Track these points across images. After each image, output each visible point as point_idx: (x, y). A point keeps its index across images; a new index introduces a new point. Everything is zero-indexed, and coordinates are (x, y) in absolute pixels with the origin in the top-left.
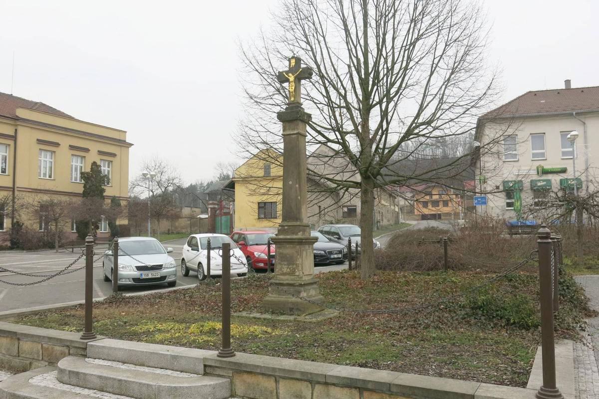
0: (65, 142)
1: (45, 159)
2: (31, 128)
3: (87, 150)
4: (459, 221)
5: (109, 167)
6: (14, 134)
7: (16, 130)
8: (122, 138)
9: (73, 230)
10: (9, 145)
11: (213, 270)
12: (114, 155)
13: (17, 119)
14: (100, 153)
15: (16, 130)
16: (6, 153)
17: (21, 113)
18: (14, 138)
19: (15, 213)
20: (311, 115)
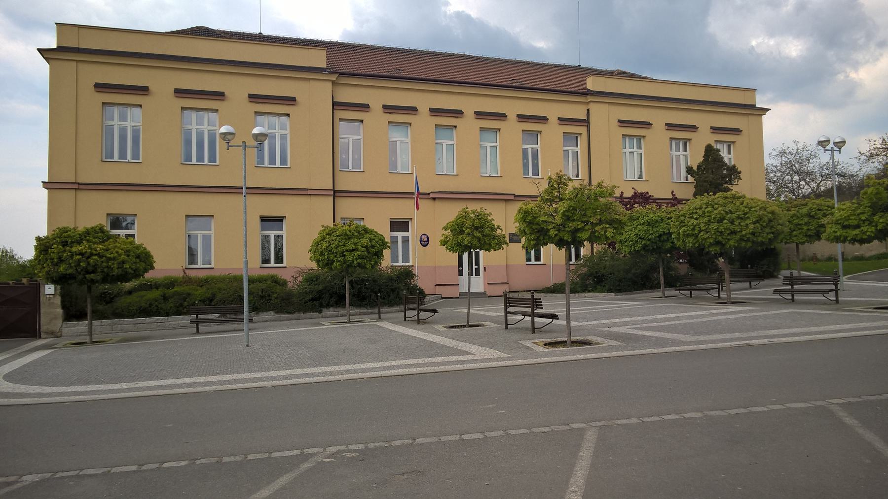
0: (659, 117)
1: (631, 150)
2: (455, 117)
3: (693, 128)
4: (703, 257)
5: (729, 153)
6: (585, 118)
7: (588, 110)
8: (749, 102)
9: (530, 260)
10: (580, 134)
11: (577, 320)
12: (737, 131)
13: (588, 93)
14: (715, 130)
15: (588, 110)
16: (577, 147)
17: (591, 83)
18: (586, 122)
19: (811, 215)
20: (224, 92)
